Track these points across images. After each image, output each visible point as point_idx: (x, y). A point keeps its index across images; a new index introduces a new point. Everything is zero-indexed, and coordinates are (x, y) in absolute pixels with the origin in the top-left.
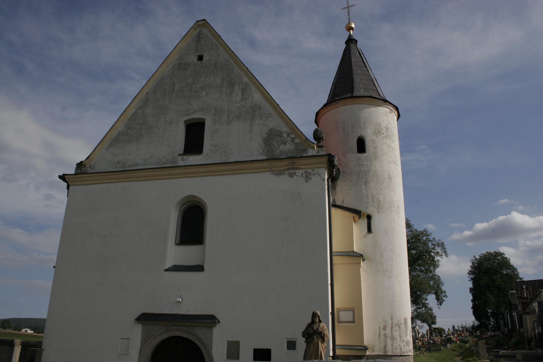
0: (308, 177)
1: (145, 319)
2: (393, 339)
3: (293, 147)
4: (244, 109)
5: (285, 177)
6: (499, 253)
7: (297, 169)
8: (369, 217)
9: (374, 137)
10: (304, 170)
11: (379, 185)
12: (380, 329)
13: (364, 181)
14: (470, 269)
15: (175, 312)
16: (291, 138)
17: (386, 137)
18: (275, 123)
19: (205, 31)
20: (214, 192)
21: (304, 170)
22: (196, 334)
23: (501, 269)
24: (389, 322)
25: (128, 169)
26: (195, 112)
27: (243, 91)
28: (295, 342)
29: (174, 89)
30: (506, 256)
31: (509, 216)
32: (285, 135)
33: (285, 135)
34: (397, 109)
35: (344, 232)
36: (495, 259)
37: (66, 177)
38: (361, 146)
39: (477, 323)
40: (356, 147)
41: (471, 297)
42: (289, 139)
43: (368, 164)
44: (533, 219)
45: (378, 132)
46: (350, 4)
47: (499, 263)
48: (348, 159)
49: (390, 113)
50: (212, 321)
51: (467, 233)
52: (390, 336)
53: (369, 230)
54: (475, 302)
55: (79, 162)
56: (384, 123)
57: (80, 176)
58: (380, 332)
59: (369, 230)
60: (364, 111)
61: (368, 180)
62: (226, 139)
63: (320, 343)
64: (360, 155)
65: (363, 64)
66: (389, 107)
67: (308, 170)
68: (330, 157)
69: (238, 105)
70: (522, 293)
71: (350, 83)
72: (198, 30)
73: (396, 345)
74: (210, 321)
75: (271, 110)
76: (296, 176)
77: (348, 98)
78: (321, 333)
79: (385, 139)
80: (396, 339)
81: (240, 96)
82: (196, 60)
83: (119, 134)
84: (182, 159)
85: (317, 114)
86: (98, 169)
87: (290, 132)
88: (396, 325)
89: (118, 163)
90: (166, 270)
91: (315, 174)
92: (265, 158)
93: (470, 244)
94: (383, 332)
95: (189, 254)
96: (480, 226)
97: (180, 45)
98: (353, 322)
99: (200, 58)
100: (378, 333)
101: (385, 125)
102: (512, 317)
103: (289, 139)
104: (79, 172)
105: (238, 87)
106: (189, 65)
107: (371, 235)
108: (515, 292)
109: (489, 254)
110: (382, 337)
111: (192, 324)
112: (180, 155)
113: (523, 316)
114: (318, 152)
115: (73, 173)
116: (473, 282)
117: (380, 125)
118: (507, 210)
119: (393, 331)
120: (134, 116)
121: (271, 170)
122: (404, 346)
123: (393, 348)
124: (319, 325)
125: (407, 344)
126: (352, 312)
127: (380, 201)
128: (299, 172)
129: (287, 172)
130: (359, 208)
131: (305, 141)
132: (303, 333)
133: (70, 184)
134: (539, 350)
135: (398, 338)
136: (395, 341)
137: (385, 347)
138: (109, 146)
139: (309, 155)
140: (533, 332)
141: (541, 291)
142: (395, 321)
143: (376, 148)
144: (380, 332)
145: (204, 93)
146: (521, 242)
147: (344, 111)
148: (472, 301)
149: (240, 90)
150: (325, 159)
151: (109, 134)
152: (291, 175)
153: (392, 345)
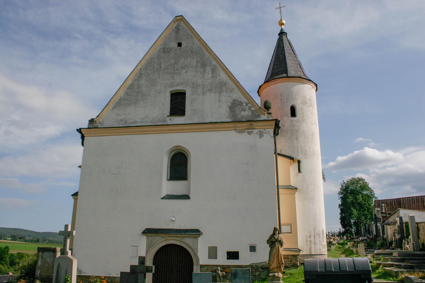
0: (261, 135)
1: (148, 232)
2: (315, 243)
3: (250, 113)
5: (245, 134)
6: (362, 179)
7: (254, 129)
8: (299, 162)
10: (258, 130)
14: (340, 190)
17: (310, 106)
18: (237, 95)
19: (182, 24)
20: (190, 141)
22: (186, 242)
23: (362, 190)
24: (313, 233)
25: (130, 125)
27: (213, 71)
30: (366, 181)
31: (362, 150)
32: (244, 105)
33: (244, 105)
35: (286, 172)
36: (358, 183)
37: (82, 130)
38: (293, 112)
39: (343, 230)
41: (340, 211)
42: (247, 107)
44: (382, 153)
45: (304, 103)
47: (360, 187)
48: (286, 121)
49: (312, 88)
50: (198, 233)
51: (332, 164)
53: (299, 171)
54: (342, 215)
55: (90, 119)
56: (306, 95)
57: (92, 130)
59: (299, 171)
60: (295, 87)
61: (298, 136)
62: (203, 105)
63: (280, 248)
64: (292, 118)
65: (292, 52)
66: (312, 84)
67: (261, 130)
68: (266, 117)
69: (209, 81)
70: (382, 210)
72: (176, 23)
73: (317, 248)
75: (234, 86)
81: (210, 75)
82: (176, 46)
83: (121, 99)
84: (170, 119)
85: (260, 87)
86: (105, 125)
89: (121, 120)
90: (162, 198)
91: (266, 133)
92: (230, 120)
93: (334, 172)
94: (309, 239)
95: (178, 187)
96: (340, 159)
97: (164, 33)
98: (291, 233)
99: (180, 45)
100: (306, 240)
101: (309, 97)
102: (376, 226)
103: (247, 107)
104: (91, 126)
105: (209, 68)
107: (300, 174)
108: (379, 209)
109: (354, 179)
110: (308, 242)
111: (183, 236)
112: (168, 116)
113: (385, 226)
114: (268, 118)
115: (87, 127)
116: (342, 200)
117: (306, 97)
118: (361, 146)
120: (131, 86)
121: (235, 129)
125: (324, 247)
127: (306, 151)
128: (255, 131)
129: (246, 131)
130: (292, 156)
132: (268, 241)
133: (85, 135)
134: (399, 249)
138: (113, 108)
139: (261, 119)
140: (393, 237)
141: (399, 210)
142: (317, 232)
143: (303, 114)
145: (184, 71)
146: (371, 170)
147: (279, 86)
148: (340, 214)
149: (210, 70)
150: (273, 123)
151: (113, 99)
152: (249, 133)
153: (315, 248)
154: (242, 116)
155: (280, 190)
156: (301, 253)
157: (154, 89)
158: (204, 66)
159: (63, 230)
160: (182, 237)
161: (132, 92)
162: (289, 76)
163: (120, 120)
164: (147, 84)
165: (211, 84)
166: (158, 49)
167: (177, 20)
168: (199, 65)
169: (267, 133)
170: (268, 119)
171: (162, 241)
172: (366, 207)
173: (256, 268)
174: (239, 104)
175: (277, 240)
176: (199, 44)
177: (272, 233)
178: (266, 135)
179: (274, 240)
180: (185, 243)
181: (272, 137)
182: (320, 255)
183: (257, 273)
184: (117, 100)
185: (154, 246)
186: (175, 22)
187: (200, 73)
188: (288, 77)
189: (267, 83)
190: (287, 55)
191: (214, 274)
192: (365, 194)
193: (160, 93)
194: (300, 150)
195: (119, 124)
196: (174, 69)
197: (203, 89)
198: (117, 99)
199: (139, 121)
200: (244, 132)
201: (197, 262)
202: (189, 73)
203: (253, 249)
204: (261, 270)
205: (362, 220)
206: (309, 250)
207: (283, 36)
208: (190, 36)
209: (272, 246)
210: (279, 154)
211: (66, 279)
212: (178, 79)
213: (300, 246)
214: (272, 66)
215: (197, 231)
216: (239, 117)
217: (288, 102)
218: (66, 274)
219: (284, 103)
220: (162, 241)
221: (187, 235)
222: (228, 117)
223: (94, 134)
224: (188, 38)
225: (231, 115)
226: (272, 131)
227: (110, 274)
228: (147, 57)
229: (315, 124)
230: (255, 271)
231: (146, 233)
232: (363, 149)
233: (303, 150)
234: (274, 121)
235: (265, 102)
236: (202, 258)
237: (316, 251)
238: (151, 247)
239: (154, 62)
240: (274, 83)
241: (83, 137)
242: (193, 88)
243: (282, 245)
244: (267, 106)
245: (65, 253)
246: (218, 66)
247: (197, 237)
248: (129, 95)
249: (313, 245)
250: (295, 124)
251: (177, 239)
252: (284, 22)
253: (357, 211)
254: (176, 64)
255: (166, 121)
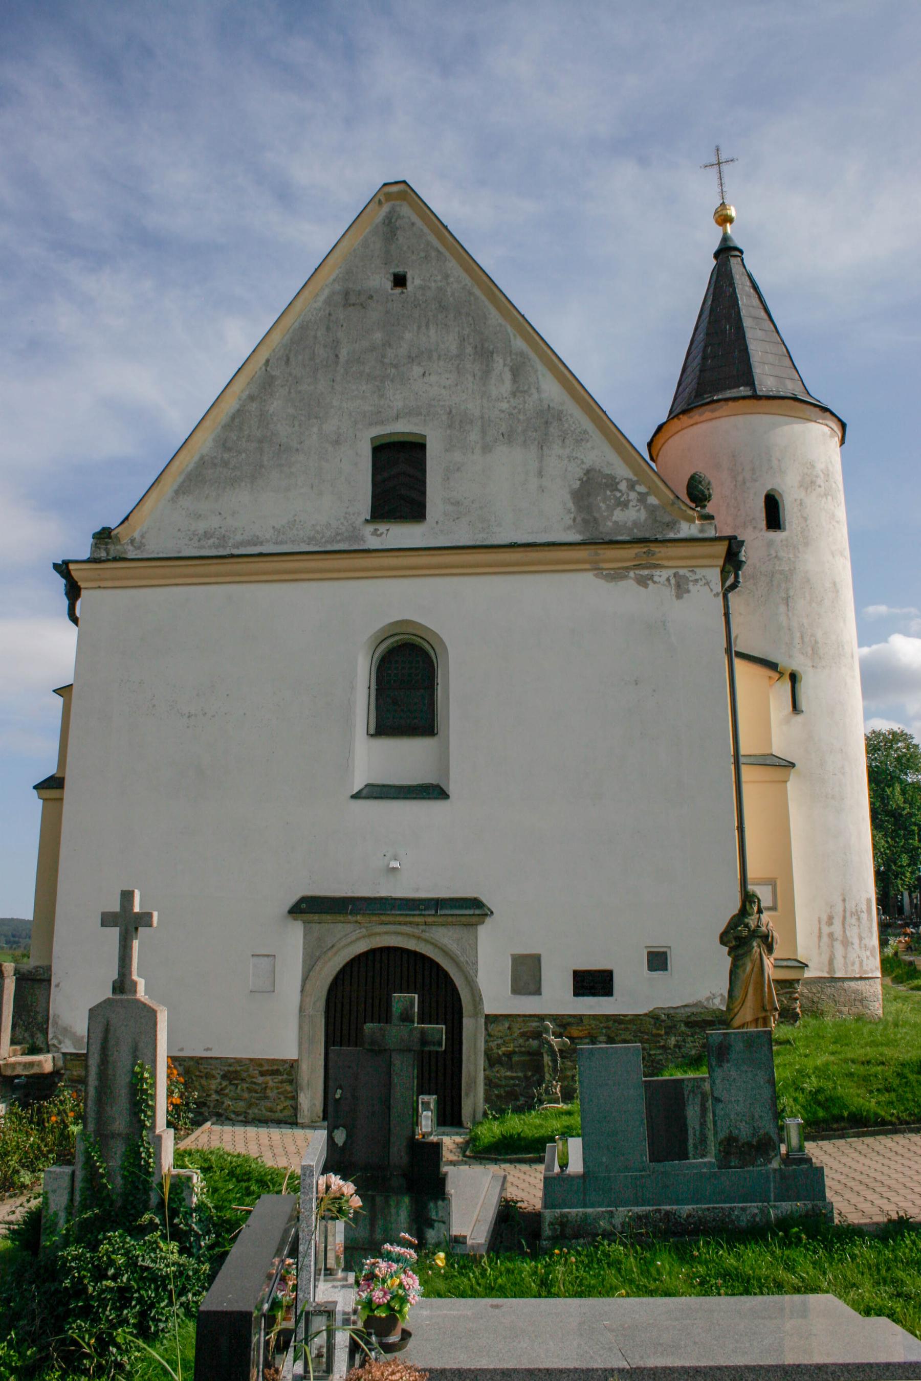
0: (681, 587)
1: (309, 908)
2: (846, 943)
3: (643, 515)
4: (521, 417)
5: (629, 585)
6: (903, 734)
7: (656, 566)
9: (802, 494)
10: (671, 572)
11: (814, 605)
12: (820, 922)
13: (784, 595)
15: (383, 893)
16: (639, 493)
17: (826, 495)
18: (599, 455)
19: (405, 210)
20: (453, 610)
21: (674, 571)
22: (437, 941)
24: (839, 908)
25: (236, 552)
26: (397, 418)
27: (516, 373)
28: (665, 954)
29: (337, 356)
30: (915, 742)
32: (623, 486)
33: (623, 486)
34: (843, 426)
36: (891, 747)
37: (71, 566)
38: (773, 513)
40: (764, 515)
42: (633, 496)
43: (791, 556)
45: (809, 483)
46: (723, 158)
47: (899, 759)
48: (756, 541)
49: (832, 436)
50: (477, 912)
52: (840, 938)
53: (795, 707)
55: (98, 529)
58: (820, 929)
59: (795, 707)
61: (791, 593)
62: (488, 485)
63: (765, 957)
65: (763, 314)
67: (682, 572)
69: (504, 405)
71: (723, 358)
72: (386, 208)
73: (852, 956)
74: (470, 911)
75: (587, 424)
76: (655, 582)
77: (744, 398)
78: (767, 936)
79: (824, 499)
80: (852, 944)
82: (389, 285)
83: (202, 463)
84: (375, 533)
85: (660, 428)
86: (154, 548)
87: (635, 479)
88: (852, 914)
89: (207, 535)
90: (354, 797)
91: (696, 581)
94: (826, 930)
95: (405, 758)
99: (400, 281)
100: (816, 931)
101: (822, 466)
104: (103, 554)
105: (501, 361)
106: (371, 297)
107: (799, 718)
110: (825, 939)
111: (430, 919)
112: (367, 521)
114: (702, 531)
115: (86, 555)
117: (813, 467)
119: (847, 927)
121: (596, 569)
122: (868, 958)
123: (846, 964)
124: (759, 918)
126: (770, 887)
127: (816, 642)
128: (661, 575)
129: (632, 574)
130: (772, 658)
131: (673, 504)
133: (82, 584)
135: (856, 941)
136: (850, 949)
137: (831, 962)
138: (177, 492)
142: (851, 906)
143: (806, 519)
144: (820, 929)
145: (417, 371)
149: (507, 369)
150: (721, 549)
151: (176, 463)
152: (643, 582)
153: (845, 957)
154: (616, 523)
155: (744, 769)
156: (808, 974)
157: (315, 429)
158: (484, 354)
159: (117, 908)
160: (426, 924)
161: (241, 437)
162: (759, 393)
163: (201, 532)
164: (291, 411)
165: (511, 414)
166: (327, 292)
167: (389, 197)
168: (469, 350)
169: (701, 583)
170: (701, 536)
171: (358, 939)
172: (915, 824)
173: (669, 1023)
174: (607, 486)
175: (754, 933)
176: (467, 280)
177: (736, 912)
178: (698, 587)
179: (745, 933)
180: (435, 945)
181: (717, 595)
182: (861, 978)
183: (672, 1041)
184: (191, 466)
185: (330, 954)
186: (380, 202)
187: (471, 379)
188: (756, 397)
189: (685, 419)
190: (747, 323)
191: (534, 1043)
192: (913, 783)
193: (337, 443)
194: (797, 640)
195: (202, 547)
196: (382, 363)
197: (484, 432)
198: (188, 461)
199: (268, 537)
200: (625, 577)
201: (475, 1007)
202: (433, 378)
203: (658, 961)
204: (683, 1028)
205: (901, 866)
206: (826, 963)
207: (733, 261)
208: (433, 254)
209: (741, 952)
210: (741, 655)
211: (135, 1074)
212: (397, 398)
213: (802, 955)
214: (698, 360)
215: (476, 903)
216: (607, 528)
217: (755, 481)
218: (136, 1058)
219: (744, 482)
220: (358, 939)
221: (440, 920)
222: (569, 528)
223: (113, 579)
224: (426, 257)
225: (579, 519)
226: (714, 575)
227: (182, 1050)
228: (289, 320)
229: (842, 555)
230: (667, 1033)
231: (302, 912)
232: (886, 641)
233: (806, 640)
234: (726, 543)
235: (692, 478)
236: (492, 990)
237: (850, 968)
238: (319, 958)
239: (315, 337)
240: (708, 415)
241: (73, 591)
242: (450, 427)
243: (770, 949)
244: (697, 493)
245: (127, 986)
246: (532, 355)
247: (475, 925)
248: (229, 450)
249: (839, 950)
250: (782, 554)
251: (407, 929)
252: (732, 212)
253: (885, 835)
254: (390, 345)
255: (362, 539)
